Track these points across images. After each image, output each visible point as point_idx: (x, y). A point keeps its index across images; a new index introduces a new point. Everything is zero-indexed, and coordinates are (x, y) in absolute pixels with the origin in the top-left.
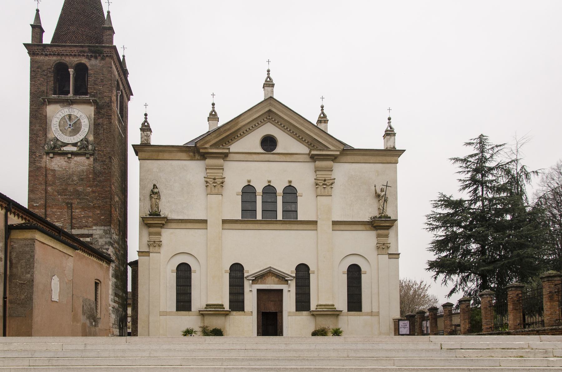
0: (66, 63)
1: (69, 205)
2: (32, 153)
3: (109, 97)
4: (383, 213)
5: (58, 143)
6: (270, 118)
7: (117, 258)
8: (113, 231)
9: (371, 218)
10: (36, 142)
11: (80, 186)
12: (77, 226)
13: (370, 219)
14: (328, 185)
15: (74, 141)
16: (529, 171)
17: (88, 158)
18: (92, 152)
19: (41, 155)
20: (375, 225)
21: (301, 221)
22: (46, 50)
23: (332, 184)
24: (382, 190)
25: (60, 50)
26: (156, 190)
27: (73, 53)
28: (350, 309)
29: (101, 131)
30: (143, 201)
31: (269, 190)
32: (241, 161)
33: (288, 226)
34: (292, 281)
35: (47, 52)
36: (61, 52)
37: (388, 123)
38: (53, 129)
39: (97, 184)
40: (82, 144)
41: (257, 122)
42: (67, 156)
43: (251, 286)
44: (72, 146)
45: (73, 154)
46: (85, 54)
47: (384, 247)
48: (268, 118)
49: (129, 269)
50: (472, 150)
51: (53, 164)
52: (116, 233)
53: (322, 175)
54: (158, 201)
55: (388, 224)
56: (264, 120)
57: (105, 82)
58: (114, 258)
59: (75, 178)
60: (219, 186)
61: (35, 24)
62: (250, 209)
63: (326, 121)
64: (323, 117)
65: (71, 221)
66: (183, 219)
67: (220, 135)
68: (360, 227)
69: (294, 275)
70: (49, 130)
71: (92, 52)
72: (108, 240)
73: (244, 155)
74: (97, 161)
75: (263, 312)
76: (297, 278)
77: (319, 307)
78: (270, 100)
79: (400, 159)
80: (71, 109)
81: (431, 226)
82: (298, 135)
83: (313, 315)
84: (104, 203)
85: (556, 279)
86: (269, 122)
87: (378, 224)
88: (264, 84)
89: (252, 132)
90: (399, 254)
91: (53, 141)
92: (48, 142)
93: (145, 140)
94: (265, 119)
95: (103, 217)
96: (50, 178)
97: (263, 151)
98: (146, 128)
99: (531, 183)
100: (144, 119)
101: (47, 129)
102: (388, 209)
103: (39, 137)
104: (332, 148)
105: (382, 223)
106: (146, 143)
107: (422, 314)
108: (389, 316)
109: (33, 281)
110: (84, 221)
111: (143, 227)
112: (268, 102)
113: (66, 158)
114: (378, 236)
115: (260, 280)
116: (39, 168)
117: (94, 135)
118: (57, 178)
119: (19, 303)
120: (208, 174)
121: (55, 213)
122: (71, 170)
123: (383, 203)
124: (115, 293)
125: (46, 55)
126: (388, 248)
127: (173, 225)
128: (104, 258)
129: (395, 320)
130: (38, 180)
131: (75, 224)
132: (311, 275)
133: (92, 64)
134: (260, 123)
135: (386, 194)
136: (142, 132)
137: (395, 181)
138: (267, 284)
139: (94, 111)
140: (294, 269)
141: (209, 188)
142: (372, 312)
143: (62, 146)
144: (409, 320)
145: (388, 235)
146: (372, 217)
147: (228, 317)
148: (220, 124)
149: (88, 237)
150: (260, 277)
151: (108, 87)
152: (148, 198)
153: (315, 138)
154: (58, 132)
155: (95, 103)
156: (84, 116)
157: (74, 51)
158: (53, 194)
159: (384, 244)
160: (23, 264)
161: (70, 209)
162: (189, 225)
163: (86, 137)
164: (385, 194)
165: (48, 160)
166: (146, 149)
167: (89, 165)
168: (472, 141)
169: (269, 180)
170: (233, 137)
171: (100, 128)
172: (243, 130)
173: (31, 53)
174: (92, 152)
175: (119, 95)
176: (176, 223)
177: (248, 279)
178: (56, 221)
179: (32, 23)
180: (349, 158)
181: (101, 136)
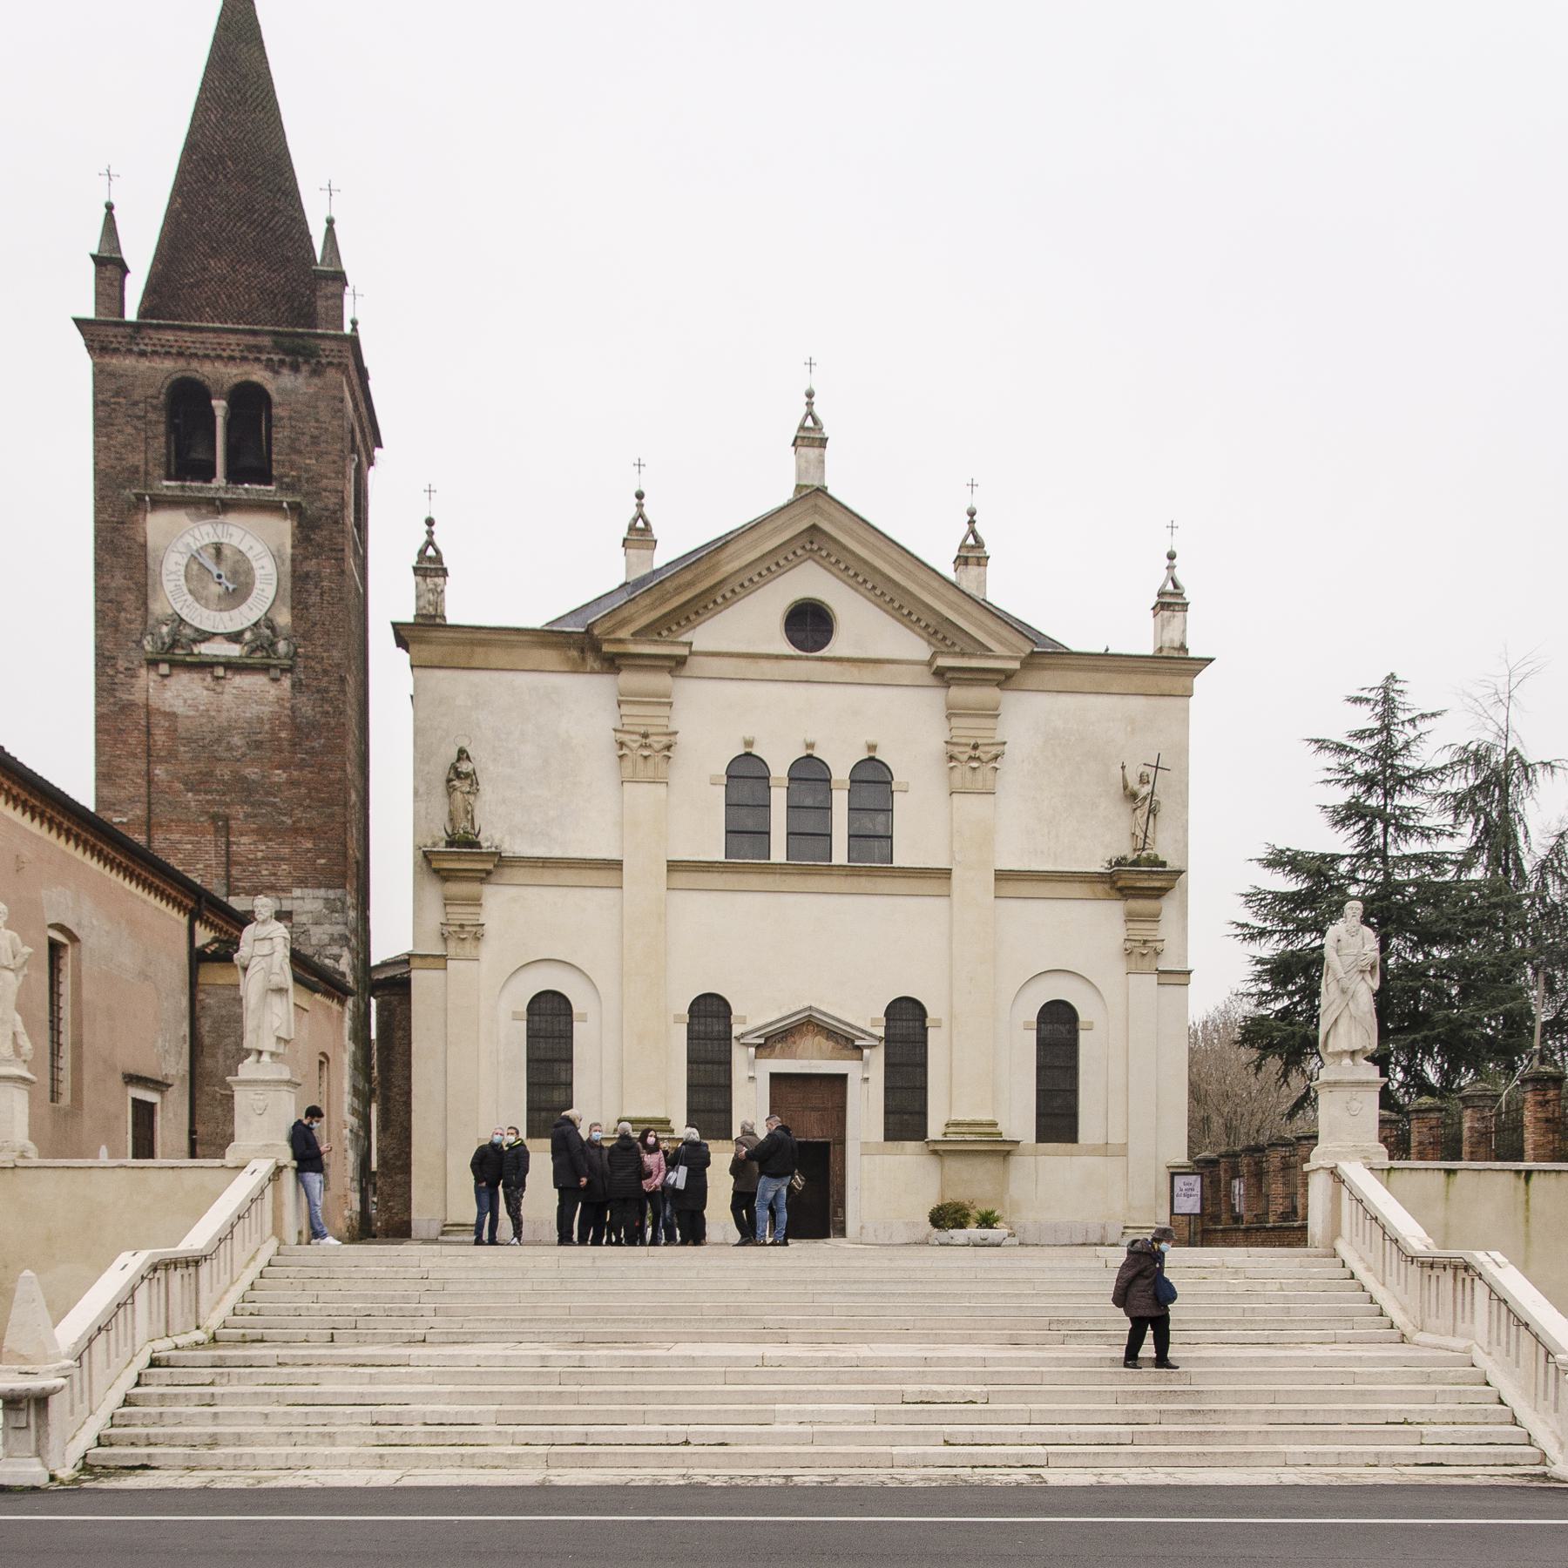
0: (204, 381)
1: (220, 823)
2: (104, 660)
3: (337, 491)
4: (1144, 849)
5: (184, 631)
6: (815, 547)
10: (116, 626)
11: (251, 766)
12: (244, 888)
13: (1106, 865)
14: (985, 760)
15: (233, 628)
16: (1529, 761)
17: (275, 680)
18: (290, 662)
19: (131, 666)
20: (1120, 884)
21: (903, 868)
22: (142, 338)
23: (996, 757)
24: (1143, 780)
25: (186, 342)
26: (465, 767)
27: (224, 350)
28: (1044, 1134)
29: (314, 599)
33: (865, 883)
34: (874, 1049)
35: (146, 345)
36: (189, 348)
37: (1167, 568)
38: (168, 586)
39: (304, 759)
40: (257, 637)
42: (212, 673)
43: (751, 1065)
44: (224, 641)
45: (232, 666)
46: (264, 357)
48: (808, 547)
50: (1366, 718)
51: (168, 694)
53: (968, 729)
54: (472, 798)
55: (1158, 884)
56: (794, 553)
57: (323, 445)
60: (658, 758)
61: (105, 255)
63: (982, 561)
64: (973, 547)
65: (228, 871)
66: (548, 856)
67: (663, 600)
68: (1077, 889)
69: (881, 1032)
70: (155, 591)
71: (287, 352)
72: (339, 929)
73: (734, 661)
74: (304, 689)
76: (889, 1040)
77: (952, 1129)
78: (812, 495)
79: (1200, 682)
80: (220, 526)
81: (1246, 931)
82: (896, 605)
83: (935, 1152)
84: (326, 820)
85: (1432, 1115)
87: (1130, 883)
89: (759, 588)
90: (1189, 972)
91: (167, 625)
92: (154, 627)
93: (430, 604)
94: (799, 552)
95: (323, 861)
96: (160, 737)
97: (791, 650)
98: (430, 567)
99: (1535, 794)
100: (425, 537)
101: (149, 588)
102: (1160, 837)
103: (124, 609)
104: (997, 648)
105: (1140, 880)
106: (433, 613)
107: (1233, 1160)
108: (1156, 1158)
110: (265, 872)
111: (426, 878)
112: (811, 502)
113: (209, 678)
114: (1131, 917)
115: (779, 1046)
116: (126, 708)
117: (293, 608)
118: (183, 738)
120: (625, 720)
121: (179, 846)
122: (225, 714)
123: (1145, 818)
125: (143, 354)
126: (1157, 953)
127: (519, 874)
129: (1171, 1170)
130: (125, 742)
131: (238, 880)
132: (930, 1031)
133: (283, 385)
134: (782, 562)
135: (1155, 790)
136: (420, 579)
137: (1184, 751)
138: (801, 1059)
139: (293, 535)
140: (881, 1014)
141: (627, 763)
143: (195, 641)
144: (1201, 1174)
145: (1158, 916)
146: (1114, 860)
150: (781, 1035)
151: (334, 462)
152: (441, 788)
153: (947, 619)
154: (185, 598)
155: (295, 508)
156: (259, 548)
157: (230, 344)
158: (170, 787)
160: (229, 1047)
161: (223, 834)
163: (268, 615)
164: (1152, 792)
165: (155, 681)
167: (279, 700)
168: (1365, 694)
169: (808, 741)
170: (702, 604)
171: (310, 587)
173: (96, 345)
174: (290, 662)
176: (527, 869)
177: (744, 1044)
179: (95, 252)
180: (1046, 677)
181: (314, 614)
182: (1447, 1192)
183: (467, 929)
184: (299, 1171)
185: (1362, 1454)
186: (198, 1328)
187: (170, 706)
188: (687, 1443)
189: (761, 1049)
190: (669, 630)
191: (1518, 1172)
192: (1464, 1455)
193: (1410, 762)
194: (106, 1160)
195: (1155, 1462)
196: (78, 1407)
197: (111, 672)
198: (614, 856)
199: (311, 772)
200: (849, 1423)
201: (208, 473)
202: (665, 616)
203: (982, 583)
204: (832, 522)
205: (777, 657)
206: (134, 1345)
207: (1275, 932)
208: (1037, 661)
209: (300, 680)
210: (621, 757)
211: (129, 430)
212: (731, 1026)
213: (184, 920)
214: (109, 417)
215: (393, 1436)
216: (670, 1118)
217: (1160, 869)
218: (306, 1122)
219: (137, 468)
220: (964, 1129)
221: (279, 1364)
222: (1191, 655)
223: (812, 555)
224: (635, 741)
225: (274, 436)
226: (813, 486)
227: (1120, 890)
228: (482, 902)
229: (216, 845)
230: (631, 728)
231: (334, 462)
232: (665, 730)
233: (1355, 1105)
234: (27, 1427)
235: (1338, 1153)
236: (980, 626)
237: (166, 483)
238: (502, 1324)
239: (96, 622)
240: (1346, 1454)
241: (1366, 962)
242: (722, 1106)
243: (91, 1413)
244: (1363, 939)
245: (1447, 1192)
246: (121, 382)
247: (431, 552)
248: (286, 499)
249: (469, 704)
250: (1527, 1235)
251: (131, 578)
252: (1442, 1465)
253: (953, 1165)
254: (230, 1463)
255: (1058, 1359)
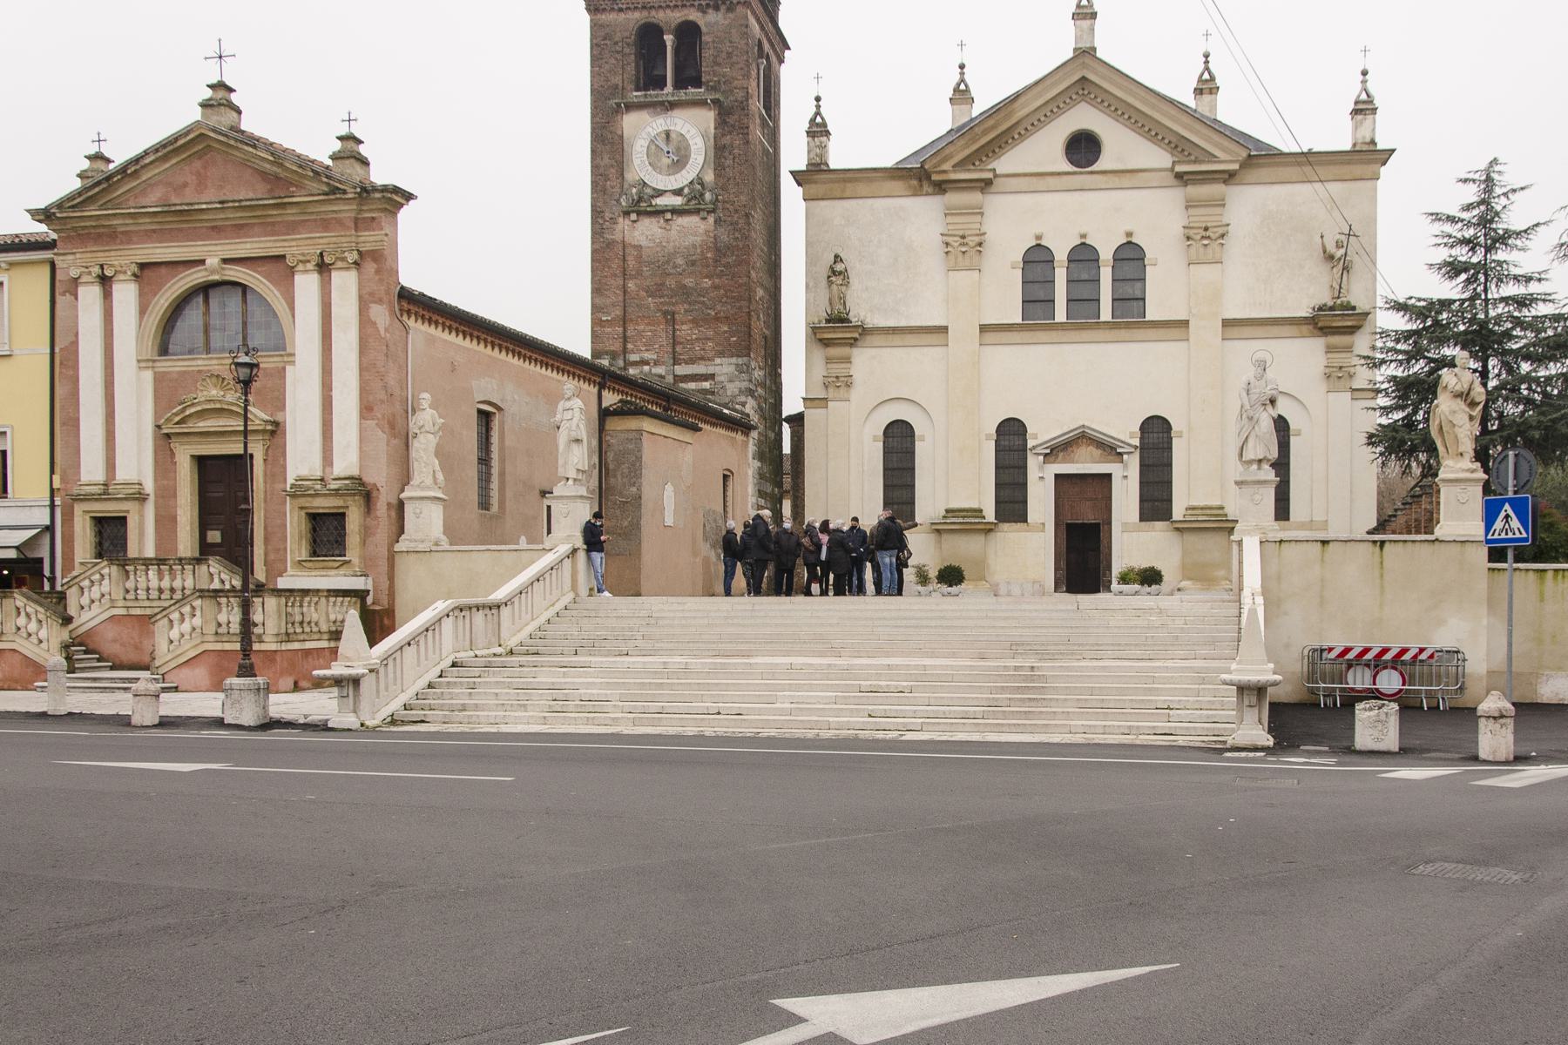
2: (596, 213)
3: (744, 88)
4: (1338, 297)
6: (1086, 92)
7: (763, 417)
8: (753, 364)
9: (1314, 309)
10: (604, 191)
12: (684, 359)
13: (1311, 311)
15: (676, 186)
17: (704, 219)
20: (1320, 325)
23: (1223, 236)
24: (1339, 245)
26: (839, 267)
29: (728, 162)
30: (813, 290)
31: (1083, 255)
32: (1021, 192)
33: (1123, 333)
34: (1131, 455)
35: (623, 4)
38: (636, 162)
39: (723, 271)
40: (692, 190)
41: (1050, 109)
43: (1041, 468)
45: (676, 211)
47: (1340, 375)
48: (1081, 92)
49: (786, 429)
50: (1471, 193)
51: (636, 233)
52: (759, 365)
53: (1202, 216)
54: (844, 288)
55: (1349, 324)
56: (1071, 98)
58: (755, 419)
59: (680, 261)
62: (1042, 298)
63: (1214, 90)
64: (1206, 81)
65: (674, 349)
67: (974, 141)
68: (1287, 330)
69: (1136, 442)
70: (628, 166)
72: (745, 384)
73: (1027, 179)
75: (1067, 524)
76: (1144, 448)
77: (1190, 512)
78: (1085, 53)
83: (1177, 529)
86: (1083, 100)
87: (1327, 324)
88: (1073, 14)
94: (1074, 97)
95: (735, 339)
96: (631, 262)
97: (1070, 168)
98: (818, 130)
100: (815, 109)
106: (819, 162)
109: (640, 497)
110: (697, 348)
113: (662, 221)
114: (1330, 349)
116: (610, 244)
119: (620, 534)
121: (643, 334)
122: (672, 244)
124: (759, 490)
125: (621, 10)
126: (1351, 376)
128: (737, 425)
130: (609, 267)
131: (680, 354)
135: (1349, 252)
136: (810, 139)
137: (1372, 221)
139: (715, 119)
140: (1137, 429)
141: (951, 257)
142: (1312, 521)
143: (653, 197)
147: (992, 535)
148: (978, 109)
149: (706, 380)
151: (742, 69)
152: (824, 282)
155: (716, 102)
156: (694, 131)
159: (1341, 368)
160: (624, 471)
161: (671, 323)
162: (910, 339)
164: (1346, 254)
166: (819, 176)
167: (707, 232)
168: (1471, 176)
169: (1082, 232)
170: (1004, 140)
171: (726, 154)
172: (1026, 124)
173: (592, 8)
175: (762, 67)
176: (883, 336)
177: (1035, 453)
178: (643, 349)
182: (1323, 557)
183: (841, 379)
184: (588, 551)
185: (1119, 726)
186: (500, 646)
187: (638, 241)
188: (719, 713)
189: (1048, 457)
190: (981, 160)
191: (1374, 542)
192: (1187, 728)
193: (1513, 219)
194: (525, 545)
195: (988, 729)
196: (392, 688)
197: (601, 222)
198: (943, 323)
199: (727, 279)
200: (820, 703)
201: (661, 83)
202: (977, 150)
203: (1214, 107)
204: (1096, 73)
205: (1059, 174)
206: (441, 654)
207: (1391, 361)
208: (1255, 161)
209: (720, 218)
210: (947, 253)
211: (613, 61)
212: (1026, 440)
213: (594, 390)
214: (600, 54)
215: (557, 706)
216: (982, 508)
217: (1350, 312)
218: (593, 521)
219: (618, 85)
220: (1209, 512)
221: (520, 666)
222: (1379, 147)
223: (1083, 98)
224: (956, 242)
225: (703, 55)
226: (1081, 48)
227: (1321, 329)
228: (852, 360)
229: (667, 332)
230: (954, 233)
231: (742, 69)
232: (978, 232)
233: (1257, 497)
234: (348, 696)
235: (1245, 530)
236: (1208, 140)
237: (635, 94)
238: (676, 645)
239: (592, 189)
240: (1109, 726)
241: (1265, 398)
242: (1021, 499)
243: (403, 691)
244: (1266, 382)
245: (1323, 557)
246: (607, 30)
247: (962, 87)
248: (710, 97)
249: (843, 223)
250: (1382, 587)
251: (614, 159)
252: (1171, 734)
253: (1191, 539)
254: (466, 720)
255: (971, 666)
